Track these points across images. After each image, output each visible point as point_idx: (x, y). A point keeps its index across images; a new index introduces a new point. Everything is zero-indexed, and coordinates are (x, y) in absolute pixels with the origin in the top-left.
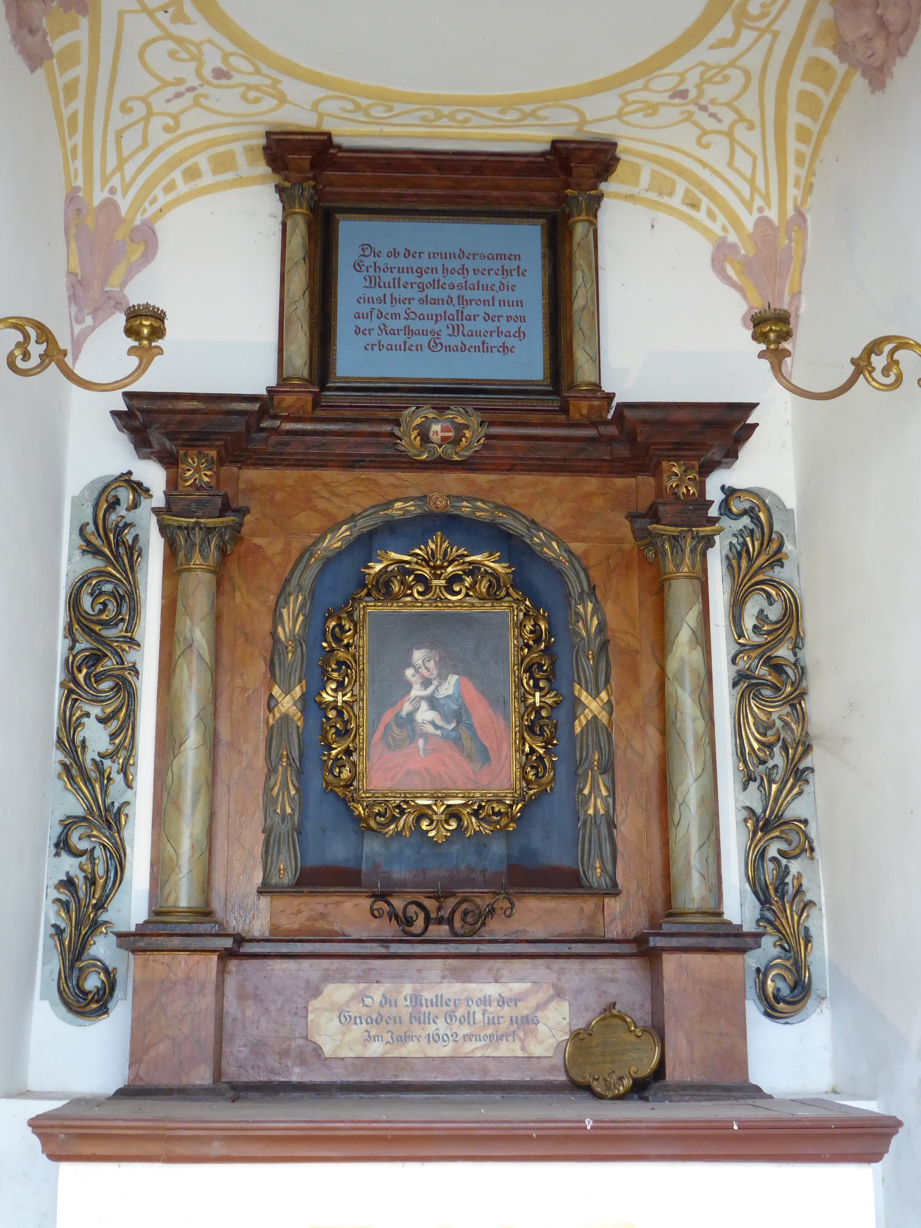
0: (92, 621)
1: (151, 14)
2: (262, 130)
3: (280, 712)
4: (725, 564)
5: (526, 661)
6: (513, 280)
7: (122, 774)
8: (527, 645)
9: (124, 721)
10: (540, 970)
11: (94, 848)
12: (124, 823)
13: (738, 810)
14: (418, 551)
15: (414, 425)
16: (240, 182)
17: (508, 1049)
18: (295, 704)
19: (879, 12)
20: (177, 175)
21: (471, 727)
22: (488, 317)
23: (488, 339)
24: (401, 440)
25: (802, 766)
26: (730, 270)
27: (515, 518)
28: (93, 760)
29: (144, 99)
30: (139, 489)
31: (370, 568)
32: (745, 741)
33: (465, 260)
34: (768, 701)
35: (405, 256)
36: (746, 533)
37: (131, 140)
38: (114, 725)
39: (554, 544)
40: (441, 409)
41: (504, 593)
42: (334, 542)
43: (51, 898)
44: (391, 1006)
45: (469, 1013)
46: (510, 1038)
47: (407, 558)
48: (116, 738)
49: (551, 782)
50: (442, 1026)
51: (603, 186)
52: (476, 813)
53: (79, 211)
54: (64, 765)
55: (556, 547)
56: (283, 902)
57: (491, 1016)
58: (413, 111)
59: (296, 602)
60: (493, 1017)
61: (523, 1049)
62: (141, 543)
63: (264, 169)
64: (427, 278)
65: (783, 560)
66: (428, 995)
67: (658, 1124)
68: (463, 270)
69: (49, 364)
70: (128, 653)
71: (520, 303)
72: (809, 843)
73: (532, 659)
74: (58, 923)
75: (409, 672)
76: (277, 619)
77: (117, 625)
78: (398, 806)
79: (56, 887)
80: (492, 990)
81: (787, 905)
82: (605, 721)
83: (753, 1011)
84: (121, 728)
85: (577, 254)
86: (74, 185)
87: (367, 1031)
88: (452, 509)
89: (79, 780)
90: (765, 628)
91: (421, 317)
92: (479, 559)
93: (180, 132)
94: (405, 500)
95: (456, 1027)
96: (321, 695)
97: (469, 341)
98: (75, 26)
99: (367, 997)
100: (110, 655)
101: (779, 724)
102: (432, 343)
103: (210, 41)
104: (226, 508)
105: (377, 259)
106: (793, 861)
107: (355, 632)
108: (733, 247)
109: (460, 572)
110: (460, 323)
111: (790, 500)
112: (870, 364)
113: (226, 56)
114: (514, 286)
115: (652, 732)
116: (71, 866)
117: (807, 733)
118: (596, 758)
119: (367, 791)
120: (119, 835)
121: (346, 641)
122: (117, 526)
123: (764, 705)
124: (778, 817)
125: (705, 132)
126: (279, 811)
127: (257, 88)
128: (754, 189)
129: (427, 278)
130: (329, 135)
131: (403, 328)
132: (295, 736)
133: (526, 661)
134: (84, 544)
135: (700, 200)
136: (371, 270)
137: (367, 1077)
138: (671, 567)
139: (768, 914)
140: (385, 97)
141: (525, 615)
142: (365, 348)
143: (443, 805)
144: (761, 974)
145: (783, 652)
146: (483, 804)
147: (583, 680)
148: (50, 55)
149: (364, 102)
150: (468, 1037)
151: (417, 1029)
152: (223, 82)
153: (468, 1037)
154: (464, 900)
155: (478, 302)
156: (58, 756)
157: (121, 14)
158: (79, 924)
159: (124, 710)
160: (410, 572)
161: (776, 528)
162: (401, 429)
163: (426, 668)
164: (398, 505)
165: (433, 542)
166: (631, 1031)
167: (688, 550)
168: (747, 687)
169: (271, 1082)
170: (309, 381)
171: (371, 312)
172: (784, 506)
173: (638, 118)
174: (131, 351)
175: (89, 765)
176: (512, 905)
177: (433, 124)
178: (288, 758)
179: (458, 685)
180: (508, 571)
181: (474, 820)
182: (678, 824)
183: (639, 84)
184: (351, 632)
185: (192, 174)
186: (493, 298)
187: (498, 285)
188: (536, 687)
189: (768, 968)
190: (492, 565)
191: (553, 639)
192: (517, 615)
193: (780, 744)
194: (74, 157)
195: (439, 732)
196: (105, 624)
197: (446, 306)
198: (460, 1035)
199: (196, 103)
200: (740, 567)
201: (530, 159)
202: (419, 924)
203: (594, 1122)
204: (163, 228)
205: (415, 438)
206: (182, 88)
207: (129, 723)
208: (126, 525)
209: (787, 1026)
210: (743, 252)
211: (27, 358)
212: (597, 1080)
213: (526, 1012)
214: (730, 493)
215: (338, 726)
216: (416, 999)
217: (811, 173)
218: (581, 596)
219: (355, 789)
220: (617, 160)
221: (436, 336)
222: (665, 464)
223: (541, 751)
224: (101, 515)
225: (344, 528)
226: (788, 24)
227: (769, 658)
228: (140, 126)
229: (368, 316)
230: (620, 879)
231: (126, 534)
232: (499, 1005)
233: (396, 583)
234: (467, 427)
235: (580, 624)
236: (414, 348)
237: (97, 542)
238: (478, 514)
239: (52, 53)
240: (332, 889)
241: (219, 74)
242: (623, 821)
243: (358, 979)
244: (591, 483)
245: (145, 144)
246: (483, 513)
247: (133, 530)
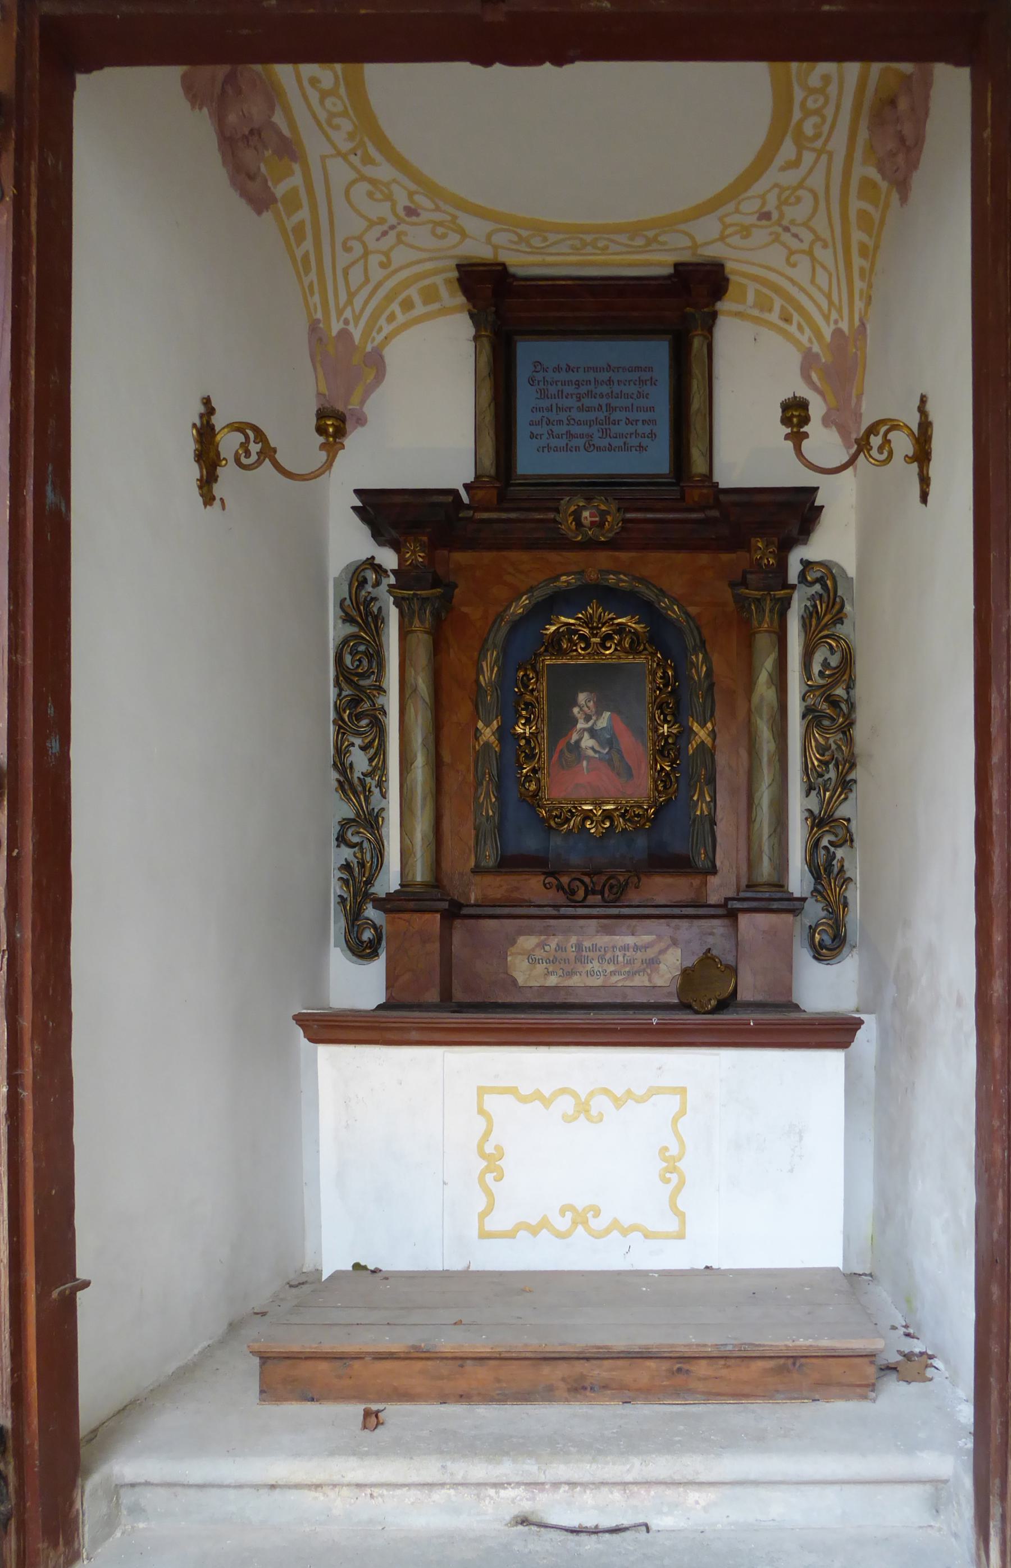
0: (351, 674)
1: (344, 156)
2: (453, 263)
3: (483, 740)
4: (801, 622)
5: (658, 700)
7: (378, 788)
8: (659, 688)
9: (377, 748)
10: (661, 927)
11: (363, 841)
12: (381, 823)
13: (802, 812)
14: (580, 615)
15: (569, 512)
16: (444, 311)
17: (640, 980)
18: (493, 734)
19: (899, 128)
20: (395, 307)
21: (619, 751)
22: (629, 422)
23: (628, 440)
24: (560, 524)
25: (848, 778)
26: (814, 377)
27: (648, 588)
28: (359, 778)
29: (359, 238)
30: (379, 570)
31: (547, 629)
32: (809, 760)
34: (826, 729)
35: (567, 371)
36: (817, 597)
37: (356, 276)
38: (372, 751)
39: (675, 607)
40: (589, 499)
41: (642, 647)
42: (519, 608)
43: (336, 878)
44: (562, 951)
45: (614, 956)
46: (641, 974)
47: (572, 621)
48: (373, 761)
49: (675, 792)
50: (596, 966)
51: (720, 306)
52: (623, 815)
53: (320, 340)
54: (338, 781)
55: (677, 610)
56: (488, 880)
57: (629, 958)
58: (563, 240)
59: (492, 655)
60: (630, 960)
61: (650, 981)
62: (383, 613)
63: (461, 299)
64: (583, 389)
65: (844, 619)
66: (587, 944)
67: (701, 1021)
68: (610, 381)
69: (264, 460)
70: (378, 698)
71: (652, 409)
72: (850, 835)
73: (662, 698)
74: (342, 894)
75: (576, 710)
76: (479, 671)
77: (369, 677)
78: (570, 811)
80: (630, 940)
81: (832, 881)
82: (710, 745)
83: (803, 957)
84: (375, 754)
85: (694, 365)
86: (315, 317)
87: (546, 968)
88: (602, 581)
89: (349, 792)
90: (827, 673)
91: (579, 423)
92: (624, 621)
93: (392, 268)
94: (568, 574)
95: (605, 966)
96: (515, 729)
98: (291, 173)
99: (547, 945)
100: (365, 699)
101: (834, 747)
103: (394, 181)
104: (436, 583)
105: (545, 373)
106: (838, 849)
107: (537, 680)
108: (817, 355)
109: (610, 632)
110: (607, 427)
111: (851, 571)
112: (868, 443)
113: (411, 195)
114: (648, 394)
115: (744, 754)
116: (349, 854)
117: (853, 754)
118: (703, 773)
119: (548, 800)
120: (378, 832)
121: (531, 687)
123: (823, 733)
124: (830, 816)
125: (792, 252)
126: (484, 814)
127: (441, 224)
128: (831, 303)
129: (583, 389)
130: (503, 265)
131: (565, 432)
132: (494, 759)
133: (658, 700)
134: (343, 614)
135: (792, 316)
136: (541, 383)
137: (546, 999)
138: (755, 623)
139: (819, 887)
140: (540, 228)
141: (658, 664)
142: (538, 450)
143: (600, 809)
144: (812, 930)
145: (840, 691)
146: (628, 808)
147: (695, 714)
148: (274, 200)
149: (525, 233)
151: (580, 967)
152: (414, 219)
154: (611, 878)
155: (621, 409)
156: (335, 775)
157: (323, 158)
158: (355, 896)
159: (377, 740)
160: (576, 632)
161: (839, 593)
162: (561, 516)
163: (588, 707)
164: (564, 578)
165: (591, 608)
166: (718, 968)
167: (767, 611)
168: (812, 718)
169: (484, 1002)
170: (497, 477)
171: (542, 420)
172: (846, 575)
173: (735, 240)
174: (323, 447)
175: (356, 781)
176: (639, 880)
177: (581, 252)
178: (490, 776)
179: (610, 718)
180: (646, 630)
181: (621, 820)
182: (755, 820)
183: (730, 207)
184: (534, 680)
185: (407, 305)
186: (632, 405)
188: (665, 721)
189: (817, 925)
190: (634, 625)
191: (677, 684)
192: (651, 665)
193: (834, 762)
194: (312, 294)
195: (597, 756)
196: (362, 676)
198: (608, 971)
199: (399, 241)
200: (811, 626)
201: (661, 282)
202: (581, 893)
203: (658, 1020)
204: (392, 355)
205: (571, 523)
206: (385, 227)
207: (382, 750)
209: (829, 966)
210: (823, 360)
211: (248, 456)
212: (695, 1001)
213: (652, 956)
214: (807, 564)
215: (527, 751)
216: (579, 947)
217: (870, 286)
218: (694, 649)
219: (539, 799)
220: (727, 280)
221: (590, 438)
222: (753, 540)
223: (668, 769)
224: (354, 592)
225: (524, 598)
226: (839, 143)
227: (829, 695)
228: (362, 262)
229: (539, 423)
230: (718, 863)
231: (373, 606)
232: (634, 951)
233: (564, 641)
234: (608, 513)
235: (693, 671)
236: (574, 449)
237: (354, 613)
238: (621, 584)
239: (276, 198)
240: (520, 870)
241: (411, 212)
242: (722, 819)
243: (541, 933)
244: (704, 558)
245: (367, 280)
246: (624, 582)
247: (377, 603)
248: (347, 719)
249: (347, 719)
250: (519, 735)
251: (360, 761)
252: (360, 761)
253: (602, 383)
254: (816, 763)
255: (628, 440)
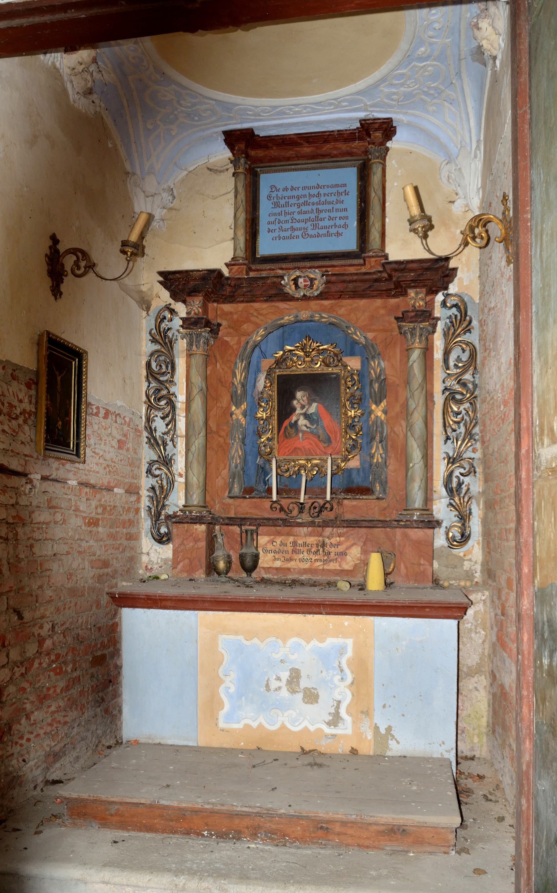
6: (342, 198)
22: (330, 219)
23: (330, 230)
33: (319, 189)
36: (454, 317)
50: (306, 555)
51: (389, 144)
61: (340, 566)
64: (302, 201)
65: (471, 330)
66: (300, 542)
71: (346, 210)
79: (148, 490)
84: (170, 422)
97: (322, 232)
101: (464, 412)
102: (304, 234)
105: (278, 192)
106: (466, 477)
122: (165, 329)
129: (302, 201)
136: (275, 199)
139: (452, 501)
145: (468, 377)
150: (316, 560)
151: (295, 556)
153: (316, 560)
179: (317, 407)
187: (335, 201)
188: (353, 408)
193: (464, 422)
195: (308, 430)
196: (163, 374)
197: (310, 215)
198: (313, 559)
208: (169, 329)
213: (342, 551)
216: (295, 543)
229: (273, 223)
236: (295, 237)
237: (158, 337)
244: (379, 302)
248: (153, 401)
249: (153, 401)
250: (259, 418)
251: (160, 425)
252: (160, 425)
253: (314, 196)
254: (451, 423)
255: (330, 230)
